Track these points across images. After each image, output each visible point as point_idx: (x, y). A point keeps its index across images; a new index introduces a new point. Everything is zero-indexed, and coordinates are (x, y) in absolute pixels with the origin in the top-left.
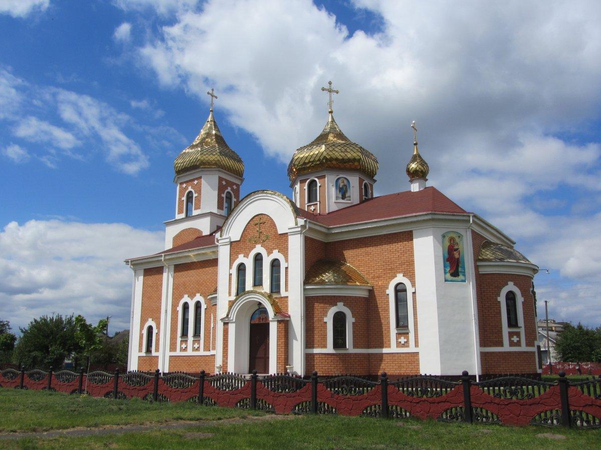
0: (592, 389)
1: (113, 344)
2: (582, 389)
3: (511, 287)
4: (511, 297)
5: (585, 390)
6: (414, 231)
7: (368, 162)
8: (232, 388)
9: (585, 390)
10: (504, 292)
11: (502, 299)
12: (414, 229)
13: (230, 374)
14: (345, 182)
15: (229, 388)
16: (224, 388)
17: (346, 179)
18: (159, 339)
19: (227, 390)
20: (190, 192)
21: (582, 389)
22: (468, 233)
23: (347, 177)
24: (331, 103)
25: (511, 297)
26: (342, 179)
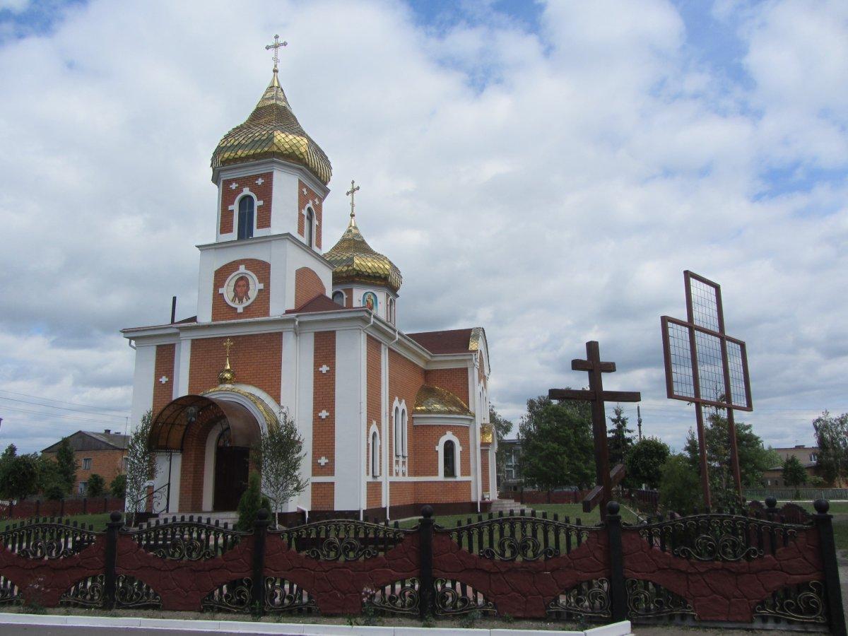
0: (475, 538)
1: (661, 468)
2: (460, 538)
3: (449, 436)
4: (449, 447)
5: (465, 541)
6: (337, 333)
7: (393, 278)
8: (57, 553)
9: (465, 541)
10: (443, 440)
11: (440, 449)
12: (338, 329)
13: (79, 526)
14: (372, 297)
15: (50, 554)
16: (39, 554)
17: (373, 294)
18: (390, 467)
19: (46, 558)
20: (243, 279)
21: (460, 538)
22: (362, 335)
23: (375, 292)
24: (276, 60)
25: (449, 447)
26: (369, 294)
